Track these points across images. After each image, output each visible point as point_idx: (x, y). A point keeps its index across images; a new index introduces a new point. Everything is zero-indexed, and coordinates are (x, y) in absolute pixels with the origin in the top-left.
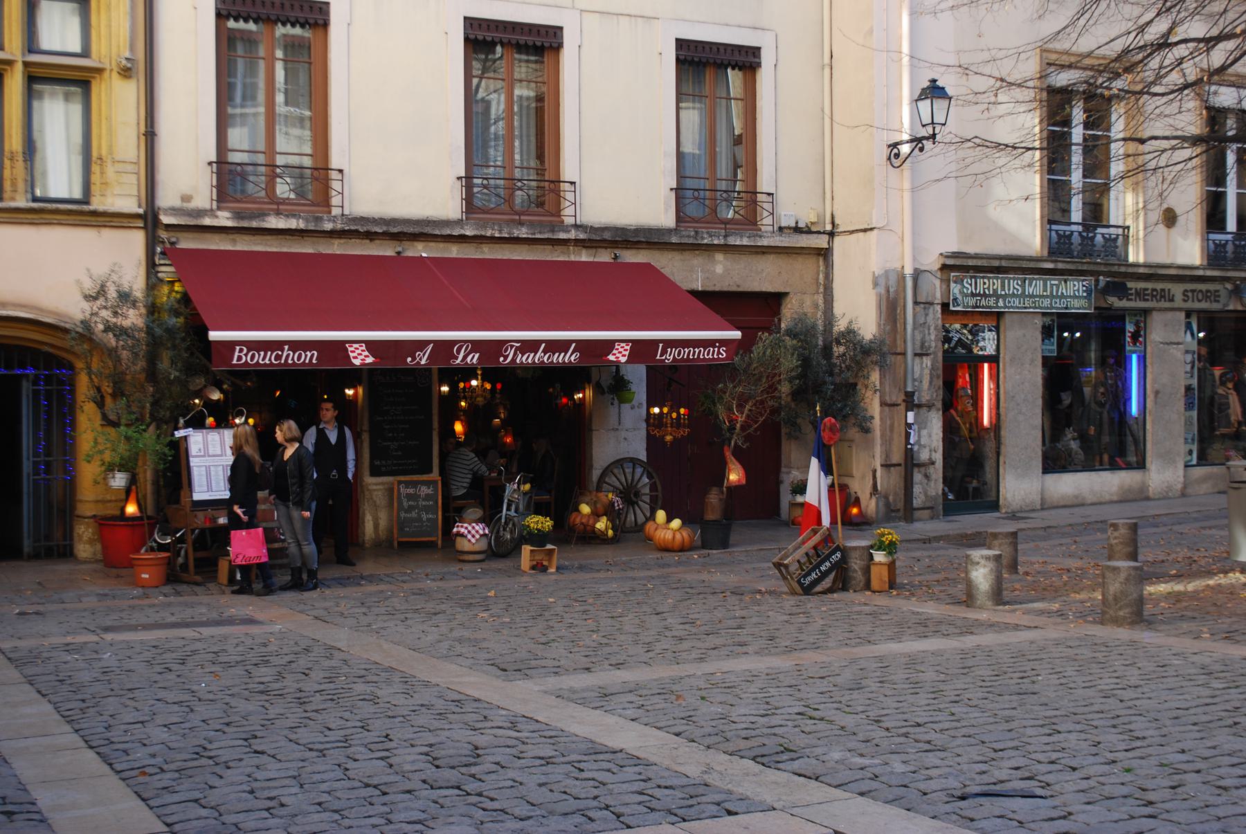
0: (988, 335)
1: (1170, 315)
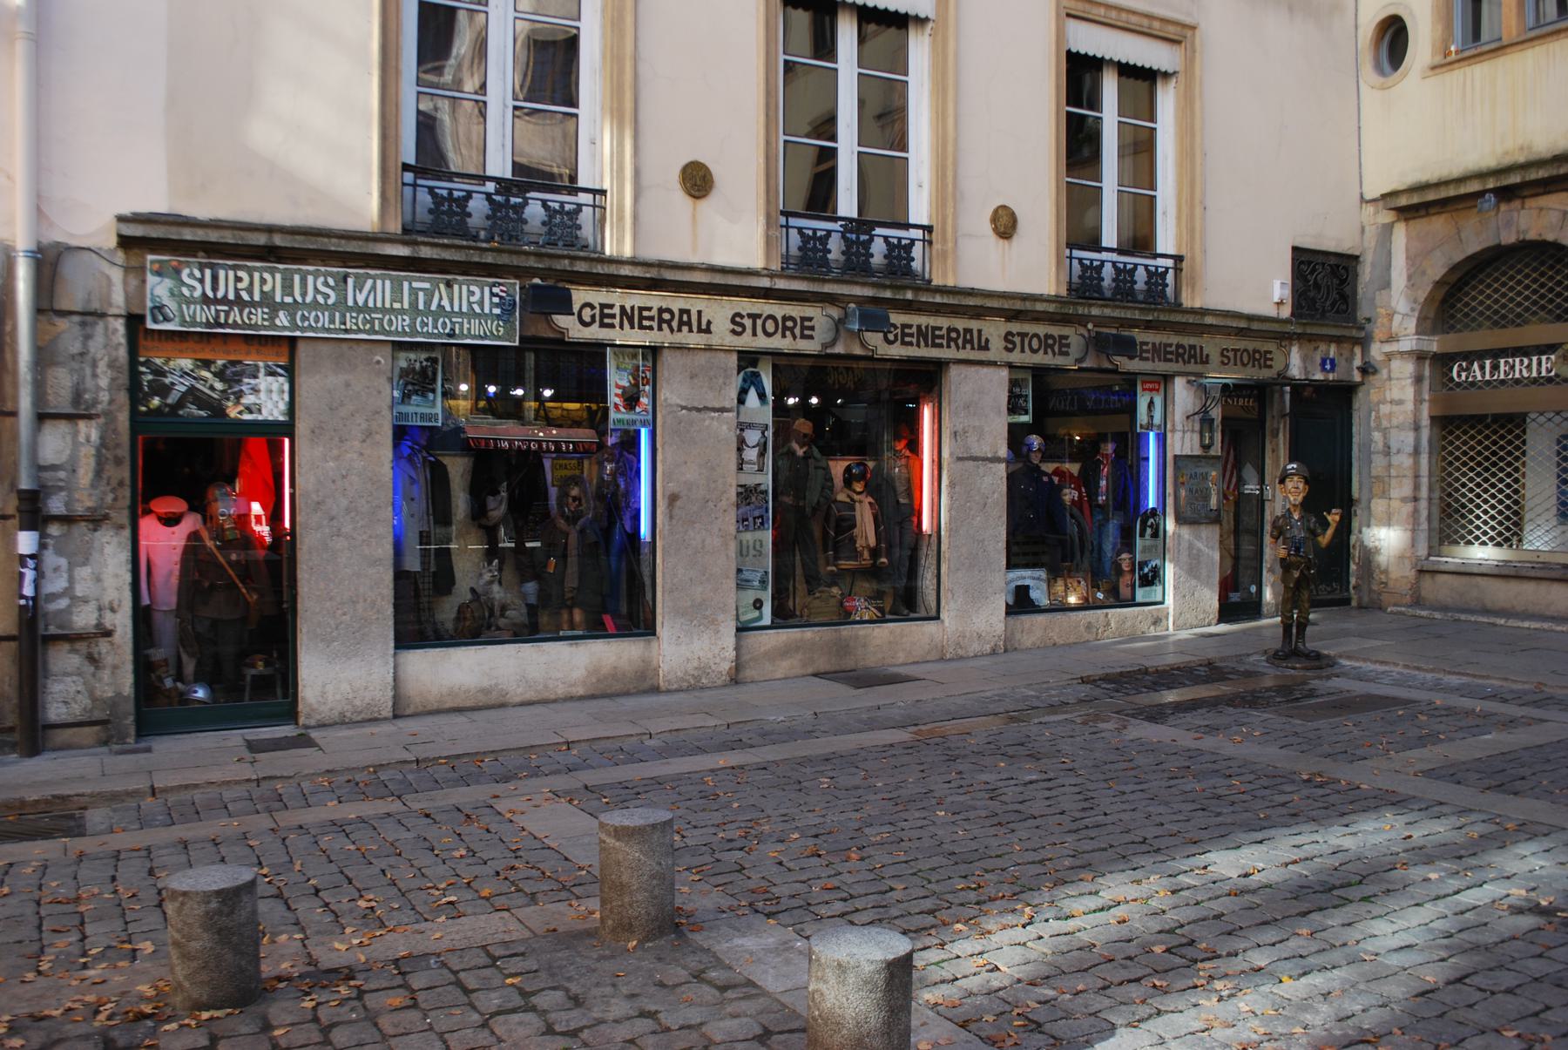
0: (264, 382)
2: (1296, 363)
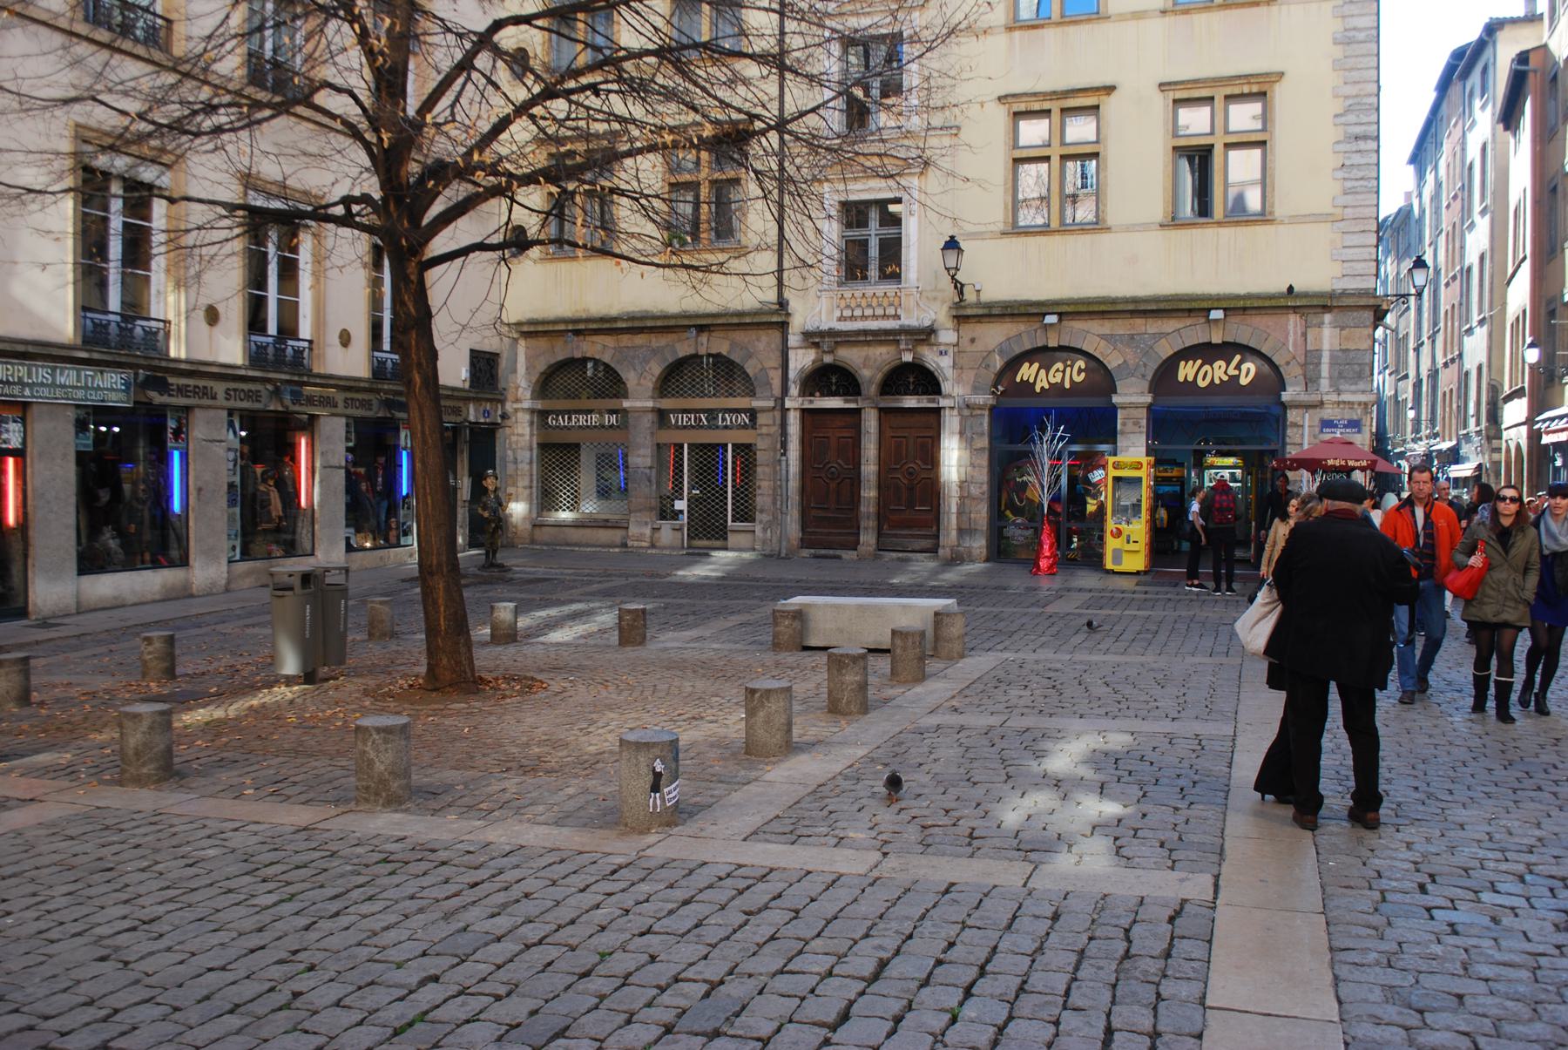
0: (13, 426)
1: (212, 413)
2: (472, 413)
